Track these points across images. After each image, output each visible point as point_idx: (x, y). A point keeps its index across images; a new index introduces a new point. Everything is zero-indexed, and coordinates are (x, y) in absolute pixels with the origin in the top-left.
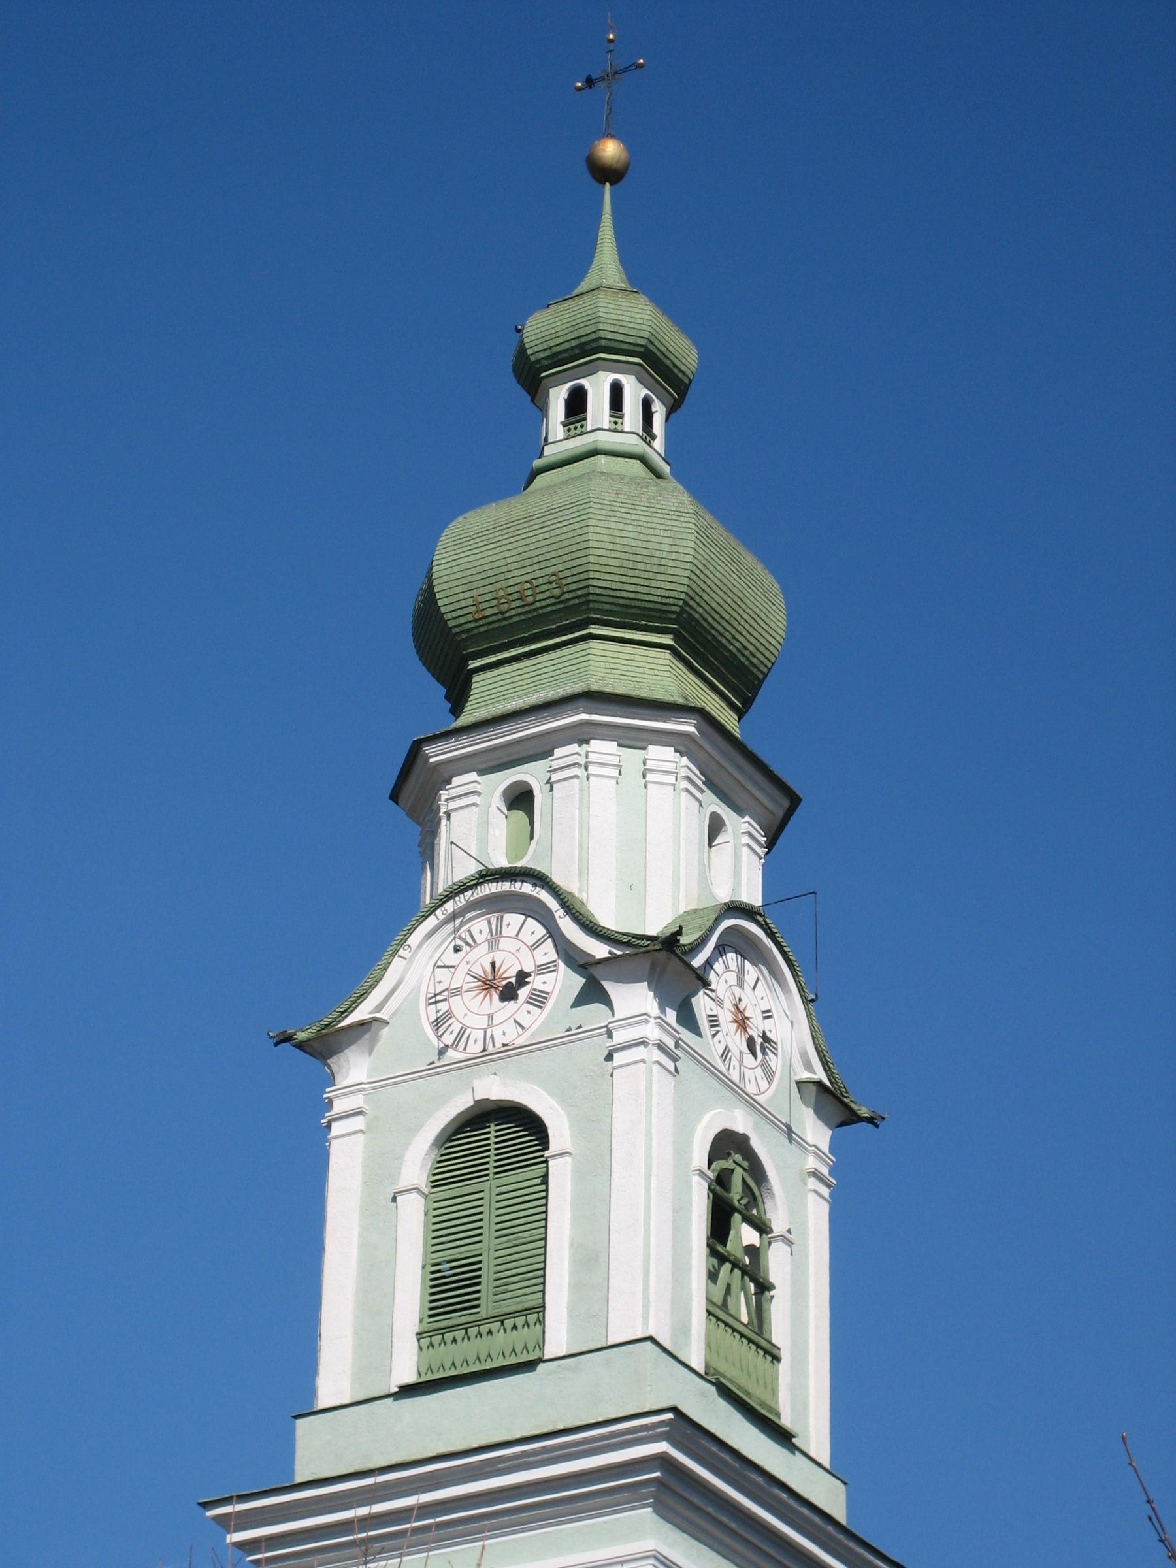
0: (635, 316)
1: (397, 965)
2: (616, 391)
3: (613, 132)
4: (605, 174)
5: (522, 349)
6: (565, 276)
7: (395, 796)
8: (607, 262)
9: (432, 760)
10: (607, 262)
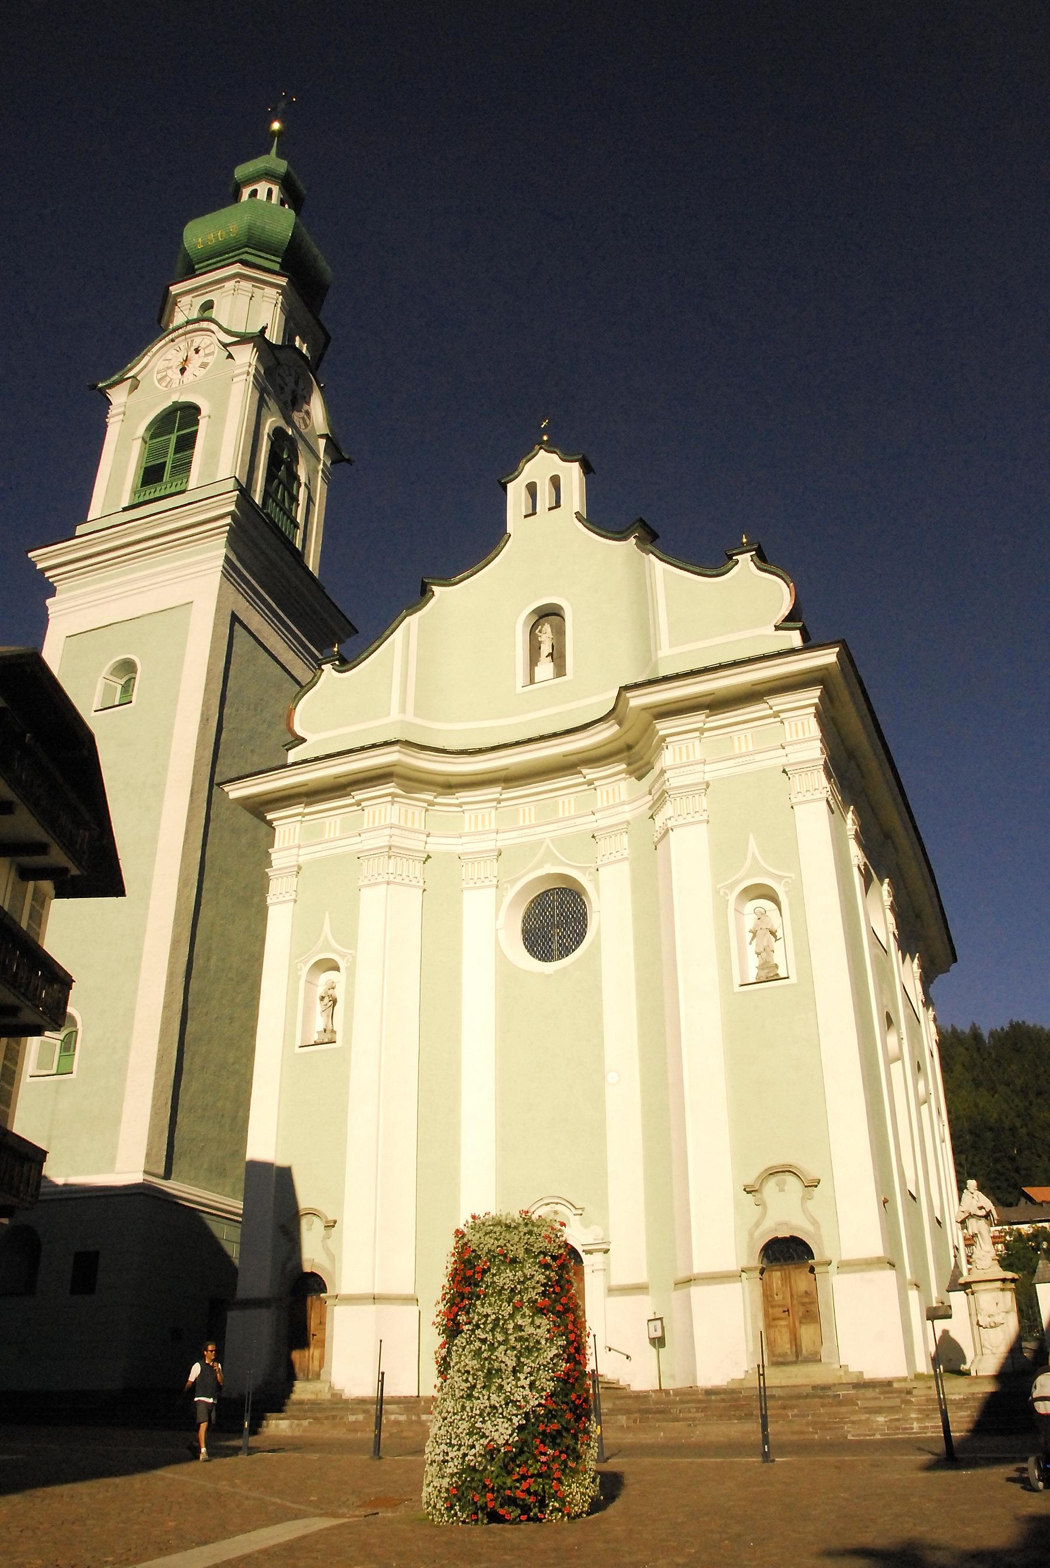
0: (282, 166)
1: (147, 358)
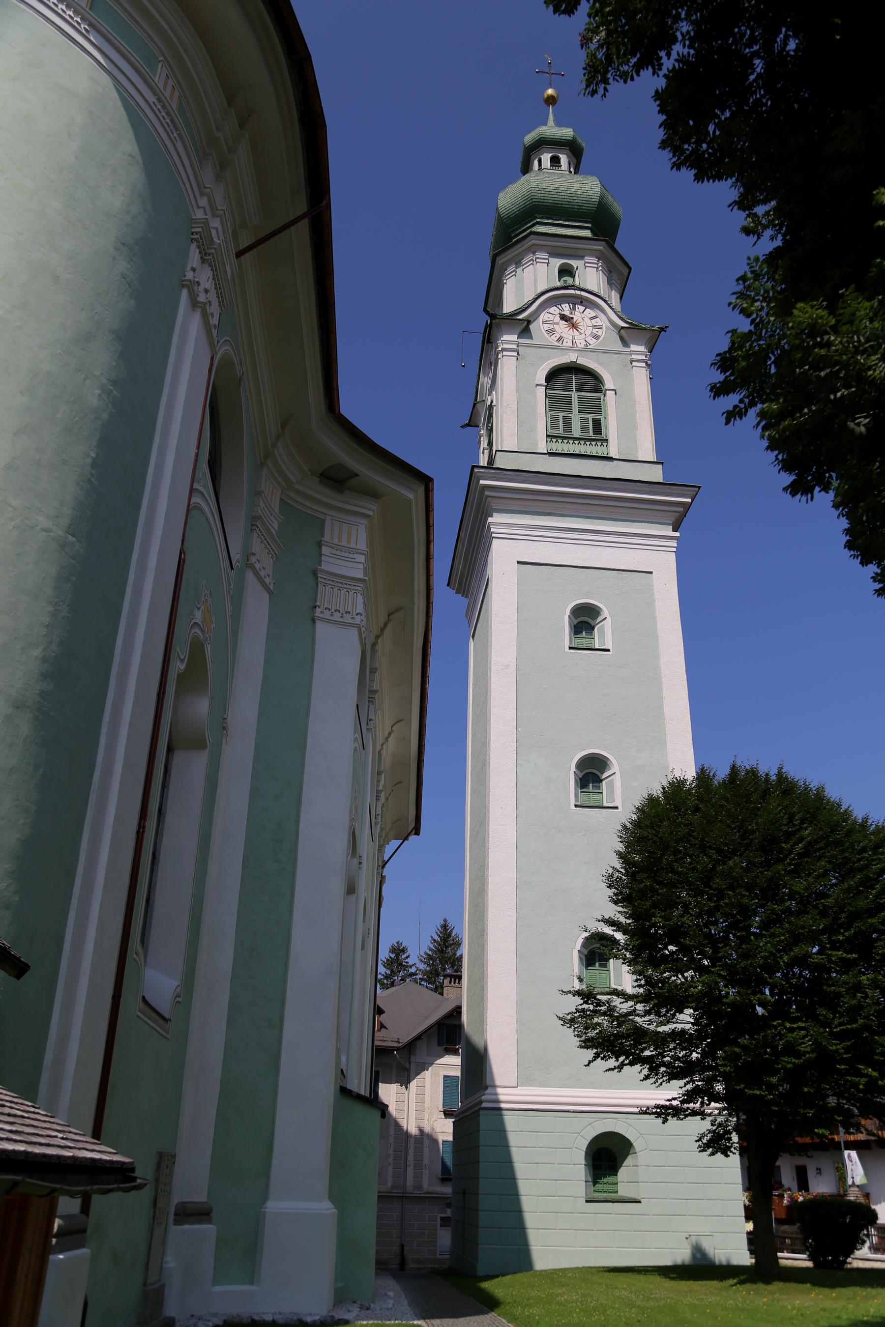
2: (544, 322)
4: (551, 100)
5: (499, 215)
8: (551, 121)
9: (482, 482)
10: (551, 121)
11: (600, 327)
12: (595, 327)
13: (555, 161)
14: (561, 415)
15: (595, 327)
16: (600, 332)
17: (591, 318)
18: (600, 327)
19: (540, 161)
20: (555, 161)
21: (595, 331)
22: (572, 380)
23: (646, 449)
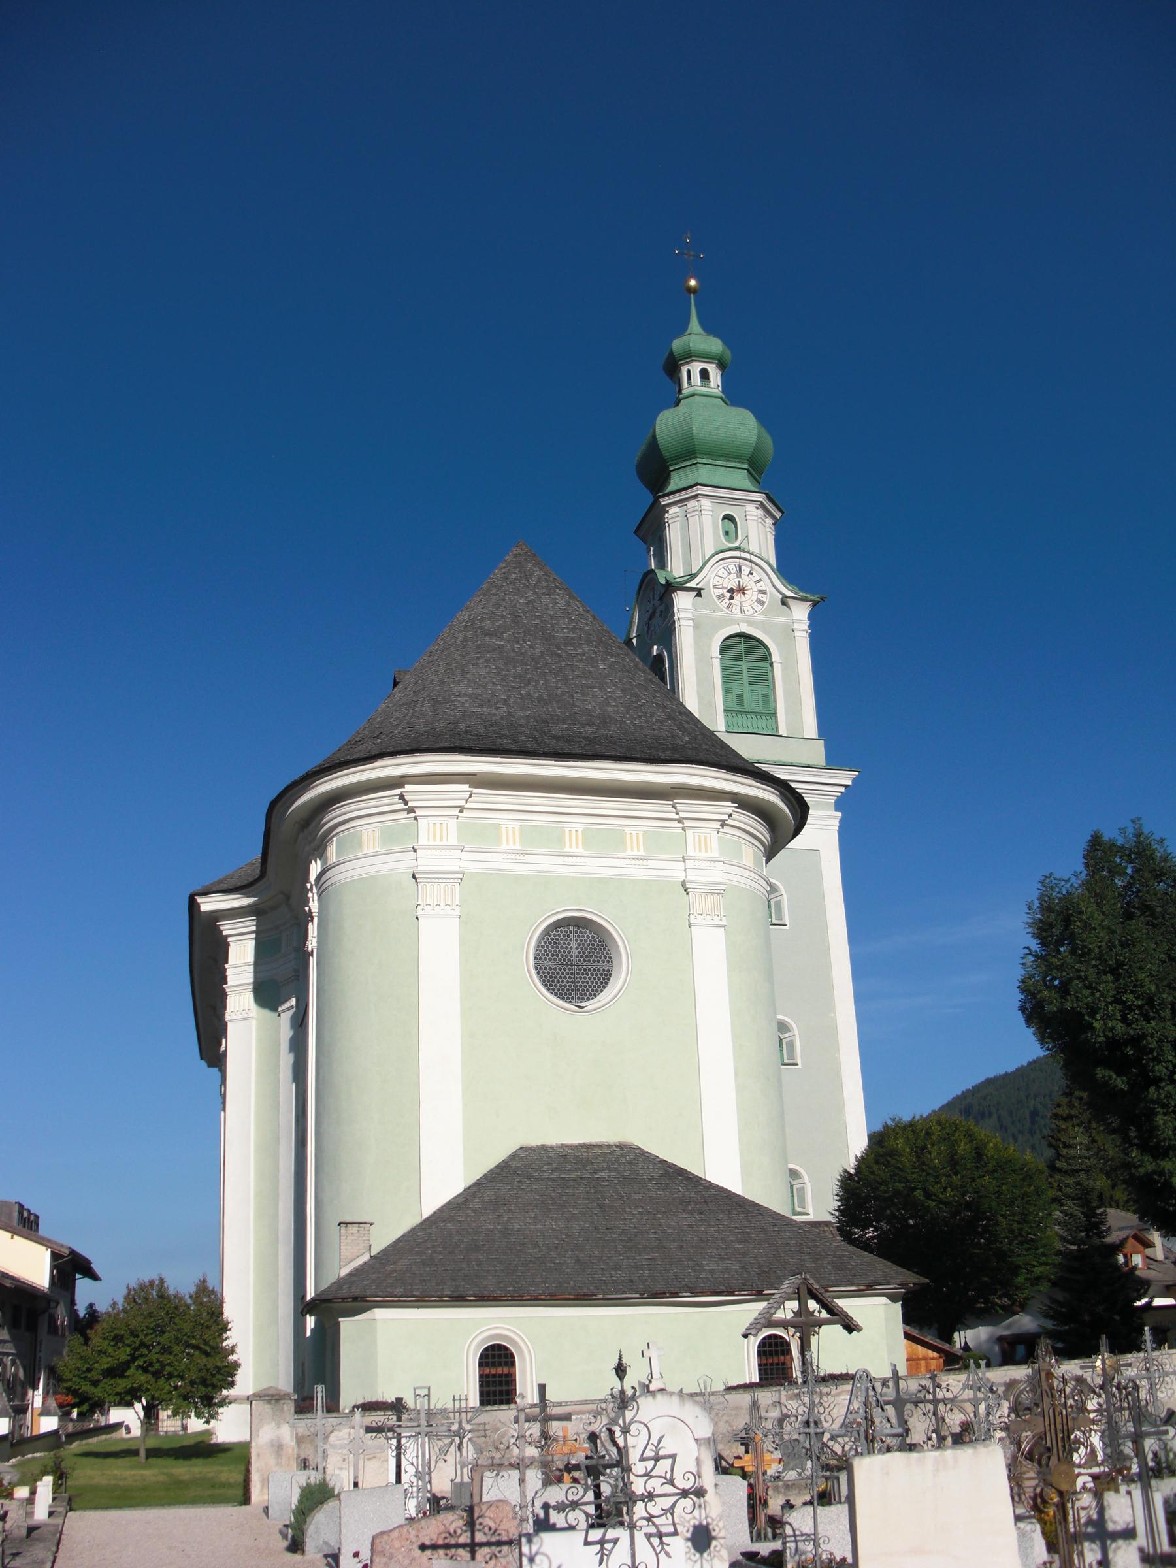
3: (768, 1218)
6: (682, 328)
7: (636, 532)
8: (694, 325)
10: (694, 325)
11: (764, 592)
12: (760, 592)
13: (704, 374)
14: (734, 687)
15: (760, 592)
16: (764, 598)
17: (757, 582)
18: (764, 592)
19: (689, 372)
20: (704, 374)
21: (760, 596)
22: (745, 651)
23: (810, 727)
